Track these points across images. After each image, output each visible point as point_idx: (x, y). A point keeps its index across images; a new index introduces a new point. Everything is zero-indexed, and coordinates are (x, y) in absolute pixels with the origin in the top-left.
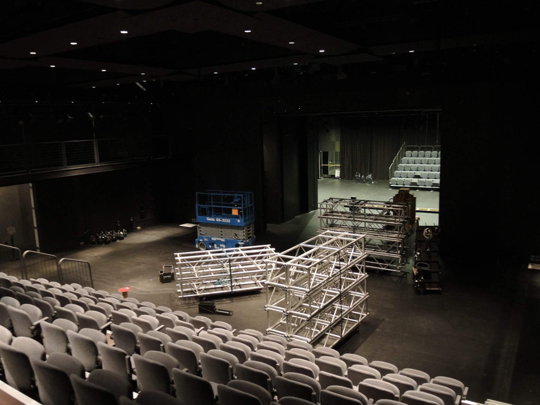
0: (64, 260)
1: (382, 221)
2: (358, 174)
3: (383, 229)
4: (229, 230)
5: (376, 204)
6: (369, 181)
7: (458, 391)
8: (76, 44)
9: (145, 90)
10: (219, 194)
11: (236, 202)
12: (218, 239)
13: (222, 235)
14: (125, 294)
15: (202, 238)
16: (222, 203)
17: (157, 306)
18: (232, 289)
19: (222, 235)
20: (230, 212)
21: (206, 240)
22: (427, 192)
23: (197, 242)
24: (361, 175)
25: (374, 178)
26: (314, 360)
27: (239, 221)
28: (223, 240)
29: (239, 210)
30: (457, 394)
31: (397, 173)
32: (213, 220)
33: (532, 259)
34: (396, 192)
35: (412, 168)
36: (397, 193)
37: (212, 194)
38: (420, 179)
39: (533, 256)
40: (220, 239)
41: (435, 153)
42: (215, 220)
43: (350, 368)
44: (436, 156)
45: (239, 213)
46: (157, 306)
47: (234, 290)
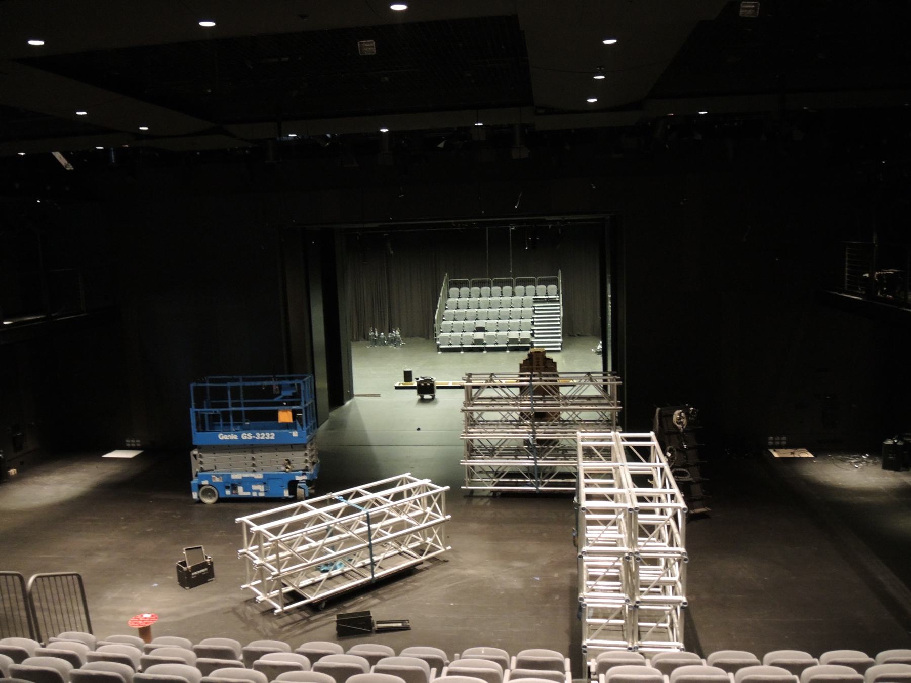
0: (35, 580)
1: (500, 408)
2: (374, 331)
3: (520, 420)
4: (241, 456)
5: (505, 379)
6: (394, 341)
7: (504, 664)
8: (42, 43)
9: (70, 168)
10: (236, 384)
11: (285, 397)
13: (254, 465)
14: (145, 632)
15: (209, 478)
16: (242, 401)
17: (196, 639)
18: (373, 574)
19: (254, 465)
20: (274, 416)
21: (217, 480)
22: (501, 354)
23: (194, 487)
24: (379, 333)
25: (406, 335)
27: (295, 434)
28: (259, 476)
29: (294, 413)
30: (431, 667)
31: (446, 325)
32: (235, 437)
33: (771, 443)
34: (524, 355)
35: (468, 316)
36: (527, 357)
37: (229, 384)
39: (127, 441)
40: (252, 475)
41: (552, 288)
42: (240, 436)
44: (555, 293)
45: (294, 418)
46: (196, 639)
47: (375, 576)
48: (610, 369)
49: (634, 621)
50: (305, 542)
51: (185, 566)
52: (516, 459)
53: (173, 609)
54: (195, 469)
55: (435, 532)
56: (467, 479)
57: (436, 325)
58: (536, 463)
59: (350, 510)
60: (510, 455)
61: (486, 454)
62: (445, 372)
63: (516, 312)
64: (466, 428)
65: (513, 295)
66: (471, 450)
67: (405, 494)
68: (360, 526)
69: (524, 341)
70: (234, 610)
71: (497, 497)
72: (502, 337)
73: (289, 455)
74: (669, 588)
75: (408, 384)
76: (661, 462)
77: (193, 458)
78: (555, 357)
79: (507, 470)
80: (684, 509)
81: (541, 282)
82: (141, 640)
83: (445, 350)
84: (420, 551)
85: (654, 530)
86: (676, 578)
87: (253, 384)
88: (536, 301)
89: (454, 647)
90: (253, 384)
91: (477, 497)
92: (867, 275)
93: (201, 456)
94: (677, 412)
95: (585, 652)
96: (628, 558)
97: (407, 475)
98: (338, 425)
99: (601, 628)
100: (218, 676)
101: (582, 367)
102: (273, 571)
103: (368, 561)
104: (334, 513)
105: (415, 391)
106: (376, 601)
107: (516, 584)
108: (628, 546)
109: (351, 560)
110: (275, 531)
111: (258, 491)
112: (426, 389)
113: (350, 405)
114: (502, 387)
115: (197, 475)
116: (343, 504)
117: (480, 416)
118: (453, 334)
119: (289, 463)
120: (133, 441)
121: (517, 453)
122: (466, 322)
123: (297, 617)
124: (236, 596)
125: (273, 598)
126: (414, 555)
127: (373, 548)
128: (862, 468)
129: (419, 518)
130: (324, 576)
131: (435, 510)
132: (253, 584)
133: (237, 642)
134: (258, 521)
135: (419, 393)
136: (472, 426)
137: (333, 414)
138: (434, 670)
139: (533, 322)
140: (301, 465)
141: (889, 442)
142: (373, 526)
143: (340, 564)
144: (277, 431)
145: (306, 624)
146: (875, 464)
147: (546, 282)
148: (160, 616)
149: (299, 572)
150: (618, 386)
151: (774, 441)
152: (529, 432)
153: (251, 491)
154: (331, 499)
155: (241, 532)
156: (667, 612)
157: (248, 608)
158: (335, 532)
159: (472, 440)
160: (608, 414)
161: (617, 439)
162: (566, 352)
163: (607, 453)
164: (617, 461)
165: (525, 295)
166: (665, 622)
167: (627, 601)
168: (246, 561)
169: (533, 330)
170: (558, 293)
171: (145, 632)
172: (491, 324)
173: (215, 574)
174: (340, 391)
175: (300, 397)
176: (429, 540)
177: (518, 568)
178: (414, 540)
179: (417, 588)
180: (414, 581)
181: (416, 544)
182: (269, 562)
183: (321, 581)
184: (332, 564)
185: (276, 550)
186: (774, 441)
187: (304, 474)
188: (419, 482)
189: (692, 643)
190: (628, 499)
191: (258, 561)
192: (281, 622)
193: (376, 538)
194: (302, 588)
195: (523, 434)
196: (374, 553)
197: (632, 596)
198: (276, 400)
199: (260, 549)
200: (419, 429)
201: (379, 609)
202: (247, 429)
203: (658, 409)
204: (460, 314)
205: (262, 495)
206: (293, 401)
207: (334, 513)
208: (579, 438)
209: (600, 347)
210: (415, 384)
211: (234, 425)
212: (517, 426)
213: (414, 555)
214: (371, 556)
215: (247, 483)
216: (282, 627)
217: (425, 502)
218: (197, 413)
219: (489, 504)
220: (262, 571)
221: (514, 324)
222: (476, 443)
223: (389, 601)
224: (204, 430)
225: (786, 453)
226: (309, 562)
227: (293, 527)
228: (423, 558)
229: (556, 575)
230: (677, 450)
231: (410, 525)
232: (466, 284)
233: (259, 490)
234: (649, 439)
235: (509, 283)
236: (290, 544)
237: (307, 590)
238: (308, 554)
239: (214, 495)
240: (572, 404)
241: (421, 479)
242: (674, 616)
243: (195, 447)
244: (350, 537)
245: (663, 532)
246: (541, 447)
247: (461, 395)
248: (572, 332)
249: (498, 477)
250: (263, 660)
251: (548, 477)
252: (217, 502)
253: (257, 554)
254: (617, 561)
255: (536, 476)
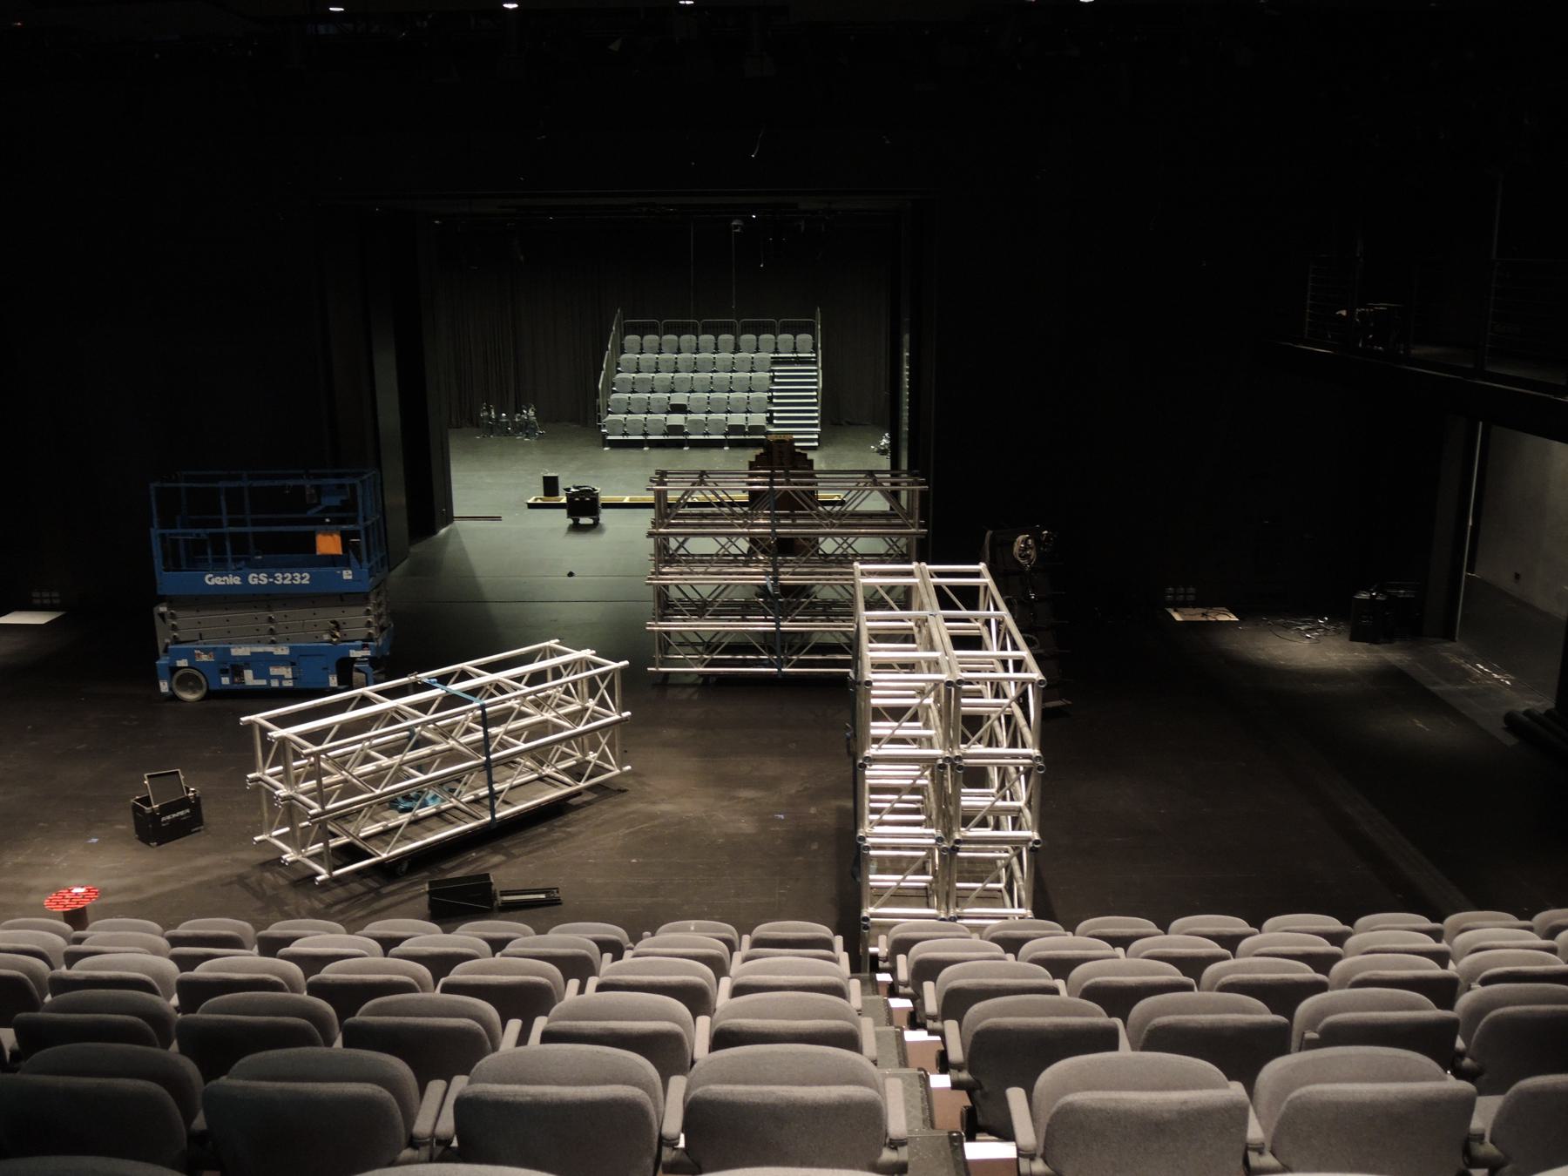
3: (751, 552)
6: (525, 428)
10: (237, 484)
11: (327, 510)
12: (260, 649)
13: (272, 632)
15: (190, 655)
18: (493, 813)
19: (272, 632)
20: (307, 544)
21: (205, 658)
24: (498, 414)
26: (304, 984)
27: (347, 575)
28: (282, 650)
29: (345, 537)
32: (237, 580)
34: (751, 454)
37: (222, 484)
38: (690, 416)
39: (36, 594)
40: (269, 649)
41: (805, 338)
42: (244, 579)
43: (312, 978)
44: (810, 348)
48: (904, 465)
49: (952, 874)
50: (368, 759)
51: (149, 805)
52: (744, 620)
53: (128, 881)
54: (163, 640)
55: (604, 741)
56: (658, 656)
57: (600, 401)
58: (778, 626)
59: (451, 701)
60: (733, 613)
61: (692, 613)
62: (621, 481)
63: (741, 379)
64: (656, 566)
65: (737, 350)
66: (666, 606)
67: (550, 676)
68: (469, 731)
69: (755, 429)
70: (241, 880)
71: (709, 684)
72: (717, 422)
73: (338, 614)
74: (1007, 821)
75: (552, 500)
76: (997, 608)
77: (158, 620)
78: (811, 455)
79: (726, 641)
80: (1041, 682)
81: (785, 329)
82: (68, 927)
83: (616, 445)
84: (576, 773)
85: (981, 726)
86: (1021, 803)
87: (267, 483)
88: (776, 362)
89: (641, 924)
90: (267, 483)
91: (676, 686)
92: (1344, 313)
93: (173, 616)
94: (1021, 538)
95: (866, 928)
96: (941, 766)
97: (553, 643)
98: (428, 568)
99: (889, 892)
100: (210, 970)
101: (856, 475)
102: (311, 808)
103: (484, 792)
104: (423, 707)
105: (564, 512)
106: (497, 859)
107: (746, 826)
108: (944, 747)
109: (453, 791)
110: (315, 737)
111: (281, 678)
112: (584, 507)
113: (448, 533)
114: (720, 505)
115: (166, 651)
116: (438, 692)
117: (681, 545)
118: (630, 417)
119: (338, 628)
120: (46, 595)
121: (744, 610)
122: (653, 396)
123: (357, 887)
124: (244, 856)
125: (313, 857)
126: (567, 779)
127: (494, 771)
128: (1318, 639)
129: (575, 717)
130: (405, 818)
131: (602, 703)
132: (275, 833)
133: (247, 925)
134: (282, 722)
135: (570, 515)
136: (668, 563)
137: (416, 549)
138: (608, 956)
139: (770, 398)
140: (359, 632)
141: (1364, 596)
142: (493, 731)
143: (434, 798)
144: (314, 570)
145: (374, 900)
146: (1338, 632)
147: (795, 330)
148: (103, 893)
149: (359, 811)
150: (921, 492)
151: (1175, 594)
152: (767, 573)
153: (269, 678)
154: (415, 684)
155: (252, 738)
156: (999, 863)
157: (268, 875)
158: (423, 742)
159: (666, 586)
160: (903, 541)
161: (923, 576)
162: (828, 451)
163: (905, 599)
164: (921, 608)
165: (757, 350)
166: (998, 881)
167: (939, 840)
168: (261, 792)
169: (771, 412)
170: (815, 350)
171: (77, 918)
172: (698, 400)
173: (205, 819)
174: (429, 507)
175: (356, 511)
176: (592, 756)
177: (746, 800)
178: (564, 756)
179: (571, 835)
180: (567, 825)
181: (570, 763)
182: (304, 793)
183: (399, 827)
184: (417, 798)
185: (316, 773)
186: (1175, 594)
187: (364, 647)
188: (576, 655)
189: (1043, 909)
190: (944, 667)
191: (283, 791)
192: (327, 897)
193: (496, 751)
194: (366, 839)
195: (757, 575)
196: (494, 778)
197: (948, 833)
198: (311, 513)
199: (286, 771)
200: (571, 574)
201: (506, 872)
202: (258, 567)
203: (989, 533)
204: (643, 381)
205: (288, 684)
206: (342, 516)
207: (423, 707)
208: (857, 573)
209: (884, 442)
210: (564, 500)
211: (235, 561)
212: (746, 564)
213: (567, 779)
214: (490, 783)
215: (261, 663)
216: (329, 906)
217: (586, 690)
218: (163, 536)
219: (695, 697)
220: (291, 811)
221: (738, 400)
222: (674, 594)
223: (524, 858)
224: (178, 568)
225: (1195, 615)
226: (378, 792)
227: (346, 730)
228: (582, 785)
229: (813, 810)
230: (1020, 602)
231: (559, 729)
232: (653, 329)
233: (284, 675)
234: (977, 575)
235: (728, 329)
236: (341, 762)
237: (374, 841)
238: (376, 779)
239: (201, 688)
240: (841, 526)
241: (579, 649)
242: (1016, 867)
243: (162, 600)
244: (451, 749)
245: (998, 730)
246: (787, 600)
247: (650, 514)
248: (838, 418)
249: (711, 653)
250: (294, 948)
251: (797, 653)
252: (204, 699)
253: (281, 781)
254: (919, 777)
255: (778, 649)
